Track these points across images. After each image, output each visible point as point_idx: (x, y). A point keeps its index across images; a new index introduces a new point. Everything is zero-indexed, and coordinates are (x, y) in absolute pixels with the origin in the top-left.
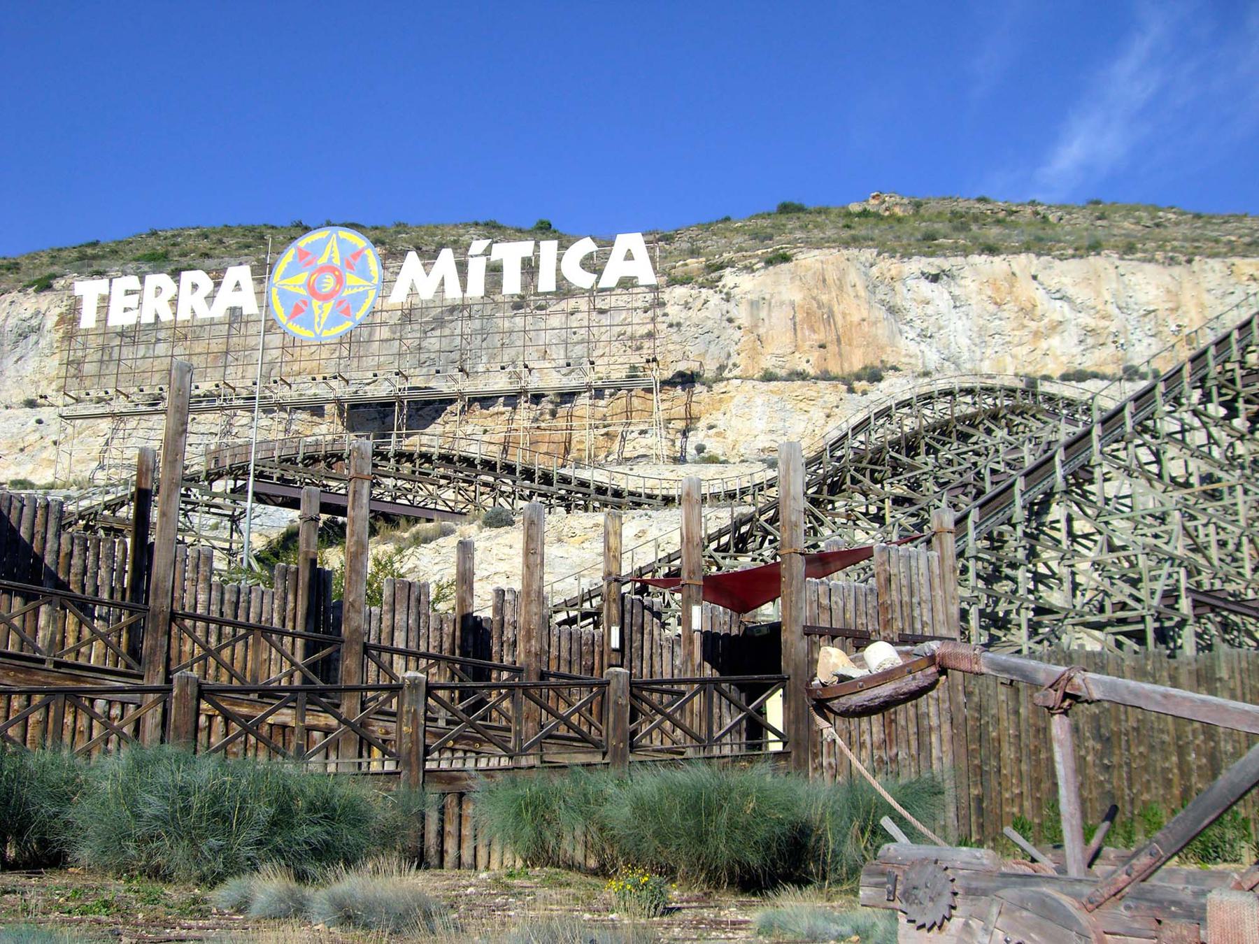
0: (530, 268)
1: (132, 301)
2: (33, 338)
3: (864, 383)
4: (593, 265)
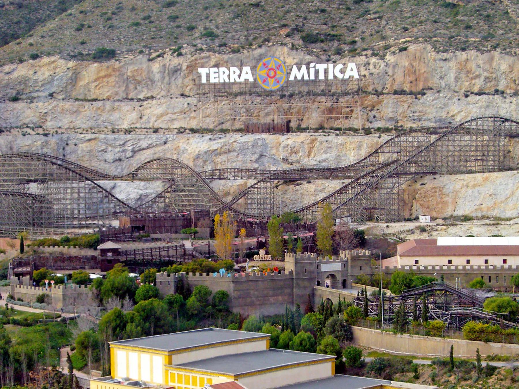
0: (326, 72)
1: (216, 75)
2: (179, 72)
3: (420, 96)
4: (342, 72)
